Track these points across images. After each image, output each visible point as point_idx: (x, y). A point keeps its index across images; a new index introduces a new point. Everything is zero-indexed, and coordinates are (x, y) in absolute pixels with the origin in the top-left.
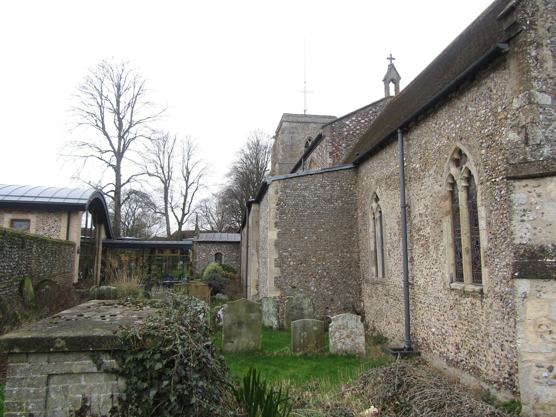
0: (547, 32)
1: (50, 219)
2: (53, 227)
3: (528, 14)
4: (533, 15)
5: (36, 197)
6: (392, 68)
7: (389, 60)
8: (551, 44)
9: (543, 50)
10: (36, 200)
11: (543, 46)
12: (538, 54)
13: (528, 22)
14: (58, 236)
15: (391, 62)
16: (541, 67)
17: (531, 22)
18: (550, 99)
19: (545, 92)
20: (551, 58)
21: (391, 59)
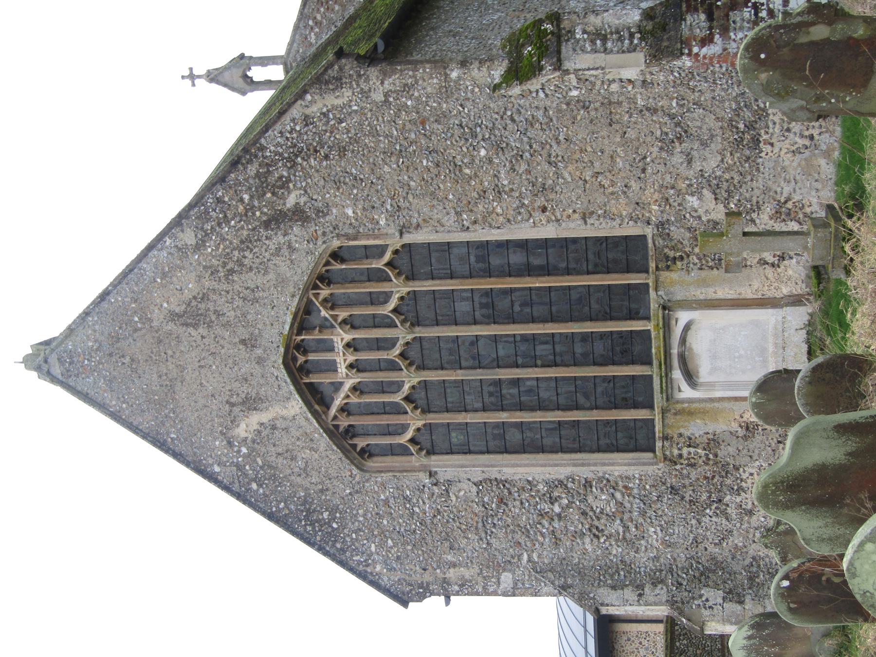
0: (427, 572)
1: (625, 649)
2: (640, 643)
3: (411, 590)
4: (411, 585)
5: (586, 631)
6: (214, 77)
7: (197, 81)
8: (441, 568)
9: (450, 578)
10: (593, 633)
11: (445, 578)
12: (456, 584)
13: (421, 590)
14: (655, 634)
15: (199, 77)
16: (471, 581)
17: (420, 587)
18: (505, 574)
19: (499, 579)
20: (457, 569)
21: (192, 77)
